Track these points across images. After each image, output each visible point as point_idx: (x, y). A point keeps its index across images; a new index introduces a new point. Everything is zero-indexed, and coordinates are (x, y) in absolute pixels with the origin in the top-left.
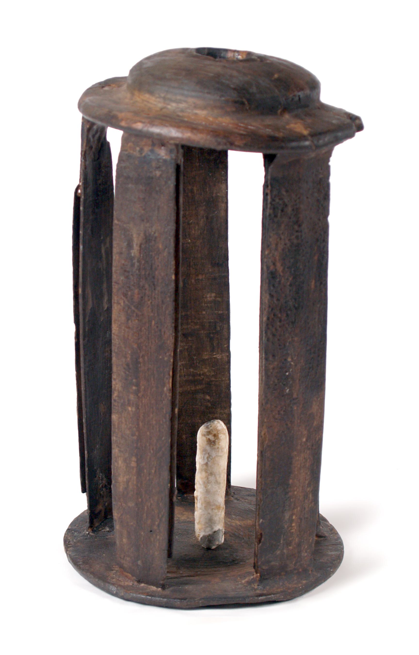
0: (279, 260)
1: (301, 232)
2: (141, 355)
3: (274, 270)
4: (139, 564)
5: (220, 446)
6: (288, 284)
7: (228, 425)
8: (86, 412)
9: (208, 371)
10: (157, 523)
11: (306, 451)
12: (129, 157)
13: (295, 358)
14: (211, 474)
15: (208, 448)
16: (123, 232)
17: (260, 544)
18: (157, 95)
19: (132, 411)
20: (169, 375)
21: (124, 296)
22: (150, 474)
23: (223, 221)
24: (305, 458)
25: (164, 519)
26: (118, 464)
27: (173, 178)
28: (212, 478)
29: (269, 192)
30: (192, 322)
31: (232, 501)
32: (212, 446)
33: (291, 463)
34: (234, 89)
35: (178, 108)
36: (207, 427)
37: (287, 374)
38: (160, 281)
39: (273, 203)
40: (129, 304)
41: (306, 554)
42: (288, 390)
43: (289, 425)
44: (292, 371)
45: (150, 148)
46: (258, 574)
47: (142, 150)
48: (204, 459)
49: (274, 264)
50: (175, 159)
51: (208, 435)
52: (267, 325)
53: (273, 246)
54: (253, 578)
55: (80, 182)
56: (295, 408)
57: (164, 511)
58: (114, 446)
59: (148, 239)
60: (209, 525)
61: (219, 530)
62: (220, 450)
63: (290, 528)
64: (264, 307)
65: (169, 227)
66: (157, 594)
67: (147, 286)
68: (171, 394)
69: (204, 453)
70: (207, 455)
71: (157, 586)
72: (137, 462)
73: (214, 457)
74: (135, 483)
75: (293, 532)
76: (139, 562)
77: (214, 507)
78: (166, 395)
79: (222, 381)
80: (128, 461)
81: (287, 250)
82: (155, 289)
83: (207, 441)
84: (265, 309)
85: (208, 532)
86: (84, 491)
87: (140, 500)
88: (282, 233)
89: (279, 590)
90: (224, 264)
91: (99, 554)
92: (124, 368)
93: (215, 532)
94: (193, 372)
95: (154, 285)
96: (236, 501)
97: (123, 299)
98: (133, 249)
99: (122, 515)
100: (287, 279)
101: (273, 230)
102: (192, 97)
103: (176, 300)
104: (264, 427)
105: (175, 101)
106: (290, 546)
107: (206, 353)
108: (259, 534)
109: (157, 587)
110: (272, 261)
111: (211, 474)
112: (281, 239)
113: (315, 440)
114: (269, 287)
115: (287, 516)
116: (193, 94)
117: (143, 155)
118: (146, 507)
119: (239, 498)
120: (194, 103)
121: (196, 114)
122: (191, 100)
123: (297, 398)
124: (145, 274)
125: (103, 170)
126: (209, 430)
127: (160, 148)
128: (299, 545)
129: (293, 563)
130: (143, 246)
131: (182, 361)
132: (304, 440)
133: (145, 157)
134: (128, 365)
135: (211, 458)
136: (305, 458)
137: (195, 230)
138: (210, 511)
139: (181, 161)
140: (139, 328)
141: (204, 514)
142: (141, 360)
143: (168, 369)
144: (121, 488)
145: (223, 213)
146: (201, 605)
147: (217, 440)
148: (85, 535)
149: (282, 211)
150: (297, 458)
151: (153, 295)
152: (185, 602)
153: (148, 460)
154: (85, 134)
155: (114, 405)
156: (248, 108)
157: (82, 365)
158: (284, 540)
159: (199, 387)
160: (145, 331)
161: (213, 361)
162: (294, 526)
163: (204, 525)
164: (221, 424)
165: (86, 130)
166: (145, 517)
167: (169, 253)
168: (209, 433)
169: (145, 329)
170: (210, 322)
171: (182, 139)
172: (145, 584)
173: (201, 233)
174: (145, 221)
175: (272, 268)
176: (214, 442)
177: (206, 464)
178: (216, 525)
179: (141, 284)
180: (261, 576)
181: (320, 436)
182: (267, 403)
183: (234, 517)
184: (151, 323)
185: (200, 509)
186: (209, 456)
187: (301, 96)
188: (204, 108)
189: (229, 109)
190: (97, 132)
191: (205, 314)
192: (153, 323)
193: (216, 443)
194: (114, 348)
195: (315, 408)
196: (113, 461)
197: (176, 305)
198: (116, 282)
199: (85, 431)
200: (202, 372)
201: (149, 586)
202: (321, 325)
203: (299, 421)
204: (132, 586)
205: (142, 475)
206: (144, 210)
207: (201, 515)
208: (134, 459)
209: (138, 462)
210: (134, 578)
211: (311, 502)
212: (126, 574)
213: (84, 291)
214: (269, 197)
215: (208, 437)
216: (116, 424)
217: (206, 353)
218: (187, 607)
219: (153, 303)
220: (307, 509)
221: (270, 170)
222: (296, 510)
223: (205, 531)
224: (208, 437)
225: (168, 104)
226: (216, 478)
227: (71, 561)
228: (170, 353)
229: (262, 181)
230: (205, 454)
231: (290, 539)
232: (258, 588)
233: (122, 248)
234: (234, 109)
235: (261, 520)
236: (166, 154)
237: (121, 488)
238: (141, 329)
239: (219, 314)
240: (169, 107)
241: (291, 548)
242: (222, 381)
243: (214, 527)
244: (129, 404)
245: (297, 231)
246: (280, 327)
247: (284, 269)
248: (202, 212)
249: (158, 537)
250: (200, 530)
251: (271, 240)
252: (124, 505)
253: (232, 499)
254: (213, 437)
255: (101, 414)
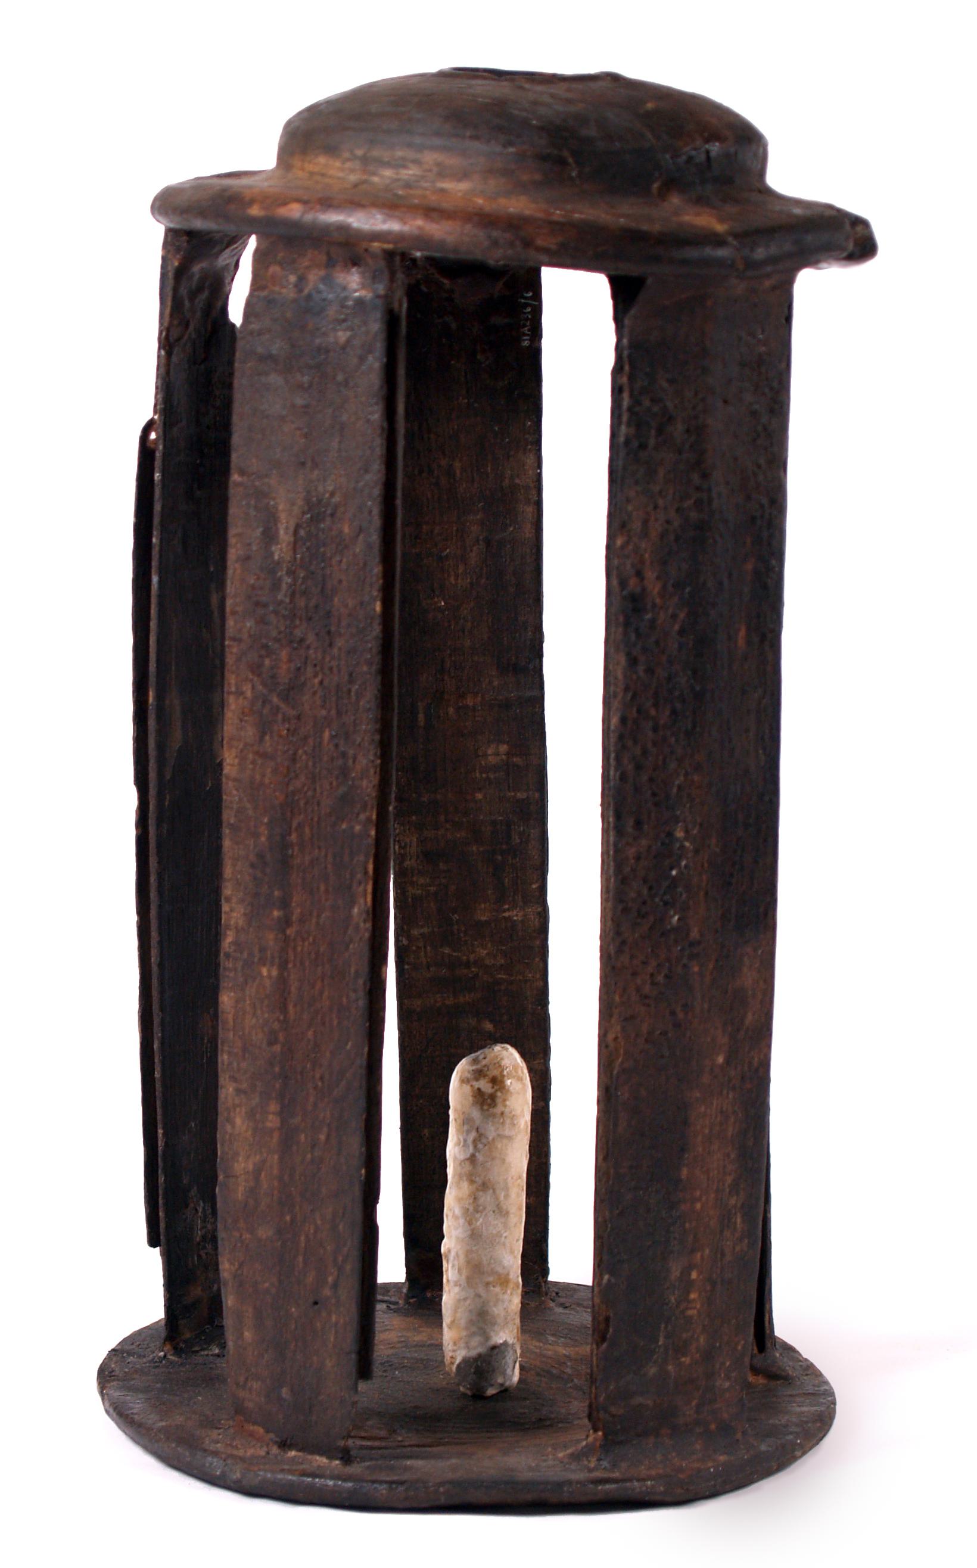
0: (652, 563)
1: (709, 490)
2: (294, 824)
3: (638, 590)
4: (284, 1396)
5: (507, 1110)
6: (677, 627)
7: (542, 1104)
8: (162, 1024)
9: (488, 954)
10: (330, 1279)
11: (725, 1092)
12: (270, 302)
13: (695, 832)
14: (485, 1186)
15: (476, 1114)
16: (253, 502)
17: (605, 1345)
18: (347, 155)
19: (270, 976)
20: (366, 873)
21: (253, 672)
22: (313, 1146)
23: (528, 551)
24: (722, 1112)
25: (348, 1267)
26: (233, 1127)
27: (379, 347)
28: (486, 1198)
29: (624, 380)
30: (447, 821)
31: (551, 1309)
32: (485, 1107)
33: (685, 1122)
34: (542, 129)
35: (398, 180)
36: (475, 1061)
37: (674, 873)
38: (344, 623)
39: (637, 409)
40: (265, 691)
41: (727, 1384)
42: (676, 918)
43: (681, 1015)
44: (686, 866)
45: (322, 273)
46: (600, 1433)
47: (302, 279)
48: (465, 1145)
49: (639, 574)
50: (386, 297)
51: (477, 1080)
52: (621, 737)
53: (636, 526)
54: (587, 1445)
55: (155, 412)
56: (696, 969)
57: (349, 1243)
58: (223, 1079)
59: (316, 512)
60: (481, 1328)
61: (505, 1343)
62: (508, 1121)
63: (683, 1305)
64: (612, 688)
65: (368, 477)
66: (328, 1472)
67: (311, 638)
68: (369, 925)
69: (466, 1127)
70: (473, 1134)
71: (329, 1453)
72: (281, 1113)
73: (491, 1138)
74: (275, 1172)
75: (691, 1317)
76: (285, 1392)
77: (491, 1279)
78: (357, 928)
79: (526, 981)
80: (258, 1116)
81: (672, 537)
82: (331, 645)
83: (474, 1096)
84: (615, 697)
85: (477, 1348)
86: (153, 1242)
87: (288, 1218)
88: (660, 492)
89: (653, 1473)
90: (531, 666)
91: (186, 1396)
92: (252, 866)
93: (494, 1348)
94: (450, 955)
95: (329, 632)
96: (560, 1310)
97: (251, 680)
98: (277, 544)
99: (241, 1265)
100: (674, 616)
101: (637, 483)
102: (433, 148)
103: (385, 672)
104: (613, 1021)
105: (388, 165)
106: (684, 1355)
107: (483, 906)
108: (601, 1318)
109: (331, 1458)
110: (633, 565)
111: (485, 1186)
112: (656, 507)
113: (750, 1063)
114: (625, 633)
115: (675, 1270)
116: (437, 141)
117: (306, 291)
118: (303, 1238)
119: (567, 1305)
120: (438, 164)
121: (443, 191)
122: (430, 158)
123: (699, 943)
124: (307, 607)
125: (217, 393)
126: (479, 1067)
127: (348, 272)
128: (708, 1356)
129: (694, 1403)
130: (302, 533)
131: (422, 927)
132: (720, 1060)
133: (309, 297)
134: (261, 856)
135: (484, 1141)
136: (722, 1112)
137: (457, 576)
138: (481, 1290)
139: (401, 305)
140: (291, 752)
141: (465, 1299)
142: (294, 837)
143: (362, 858)
144: (241, 1189)
145: (528, 531)
146: (443, 1500)
147: (499, 1094)
148: (156, 1359)
149: (660, 431)
150: (703, 1109)
151: (327, 659)
152: (401, 1488)
153: (310, 1108)
154: (171, 282)
155: (224, 968)
156: (574, 174)
157: (153, 895)
158: (667, 1337)
159: (465, 998)
160: (304, 757)
161: (503, 927)
162: (694, 1300)
163: (467, 1328)
164: (512, 1054)
165: (171, 275)
166: (301, 1265)
167: (369, 546)
168: (479, 1074)
169: (306, 753)
170: (494, 823)
171: (400, 237)
172: (300, 1450)
173: (471, 584)
174: (309, 464)
175: (633, 582)
176: (493, 1097)
177: (472, 1159)
178: (496, 1328)
179: (298, 633)
180: (605, 1435)
181: (762, 1057)
182: (620, 951)
183: (551, 1338)
184: (321, 737)
185: (456, 1284)
186: (480, 1136)
187: (713, 154)
188: (464, 175)
189: (525, 178)
190: (199, 289)
191: (480, 801)
192: (326, 735)
193: (499, 1101)
194: (228, 816)
195: (748, 978)
196: (220, 1119)
197: (383, 683)
198: (234, 639)
199: (157, 1075)
200: (472, 957)
201: (310, 1457)
202: (764, 749)
203: (706, 1006)
204: (264, 1457)
205: (295, 1148)
206: (306, 436)
207: (459, 1301)
208: (274, 1107)
209: (285, 1113)
210: (272, 1435)
211: (741, 1240)
212: (251, 1428)
213: (159, 697)
214: (626, 395)
215: (476, 1085)
216: (230, 1017)
217: (483, 906)
218: (407, 1504)
219: (326, 683)
220: (728, 1257)
221: (627, 321)
222: (699, 1255)
223: (467, 1347)
224: (476, 1085)
225: (374, 174)
226: (497, 1198)
227: (111, 1410)
228: (368, 814)
229: (608, 359)
230: (468, 1132)
231: (684, 1335)
232: (594, 1468)
233: (249, 544)
234: (538, 177)
235: (606, 1277)
236: (363, 286)
237: (241, 1189)
238: (295, 754)
239: (518, 801)
240: (376, 179)
241: (686, 1360)
242: (526, 981)
243: (492, 1334)
244: (263, 962)
245: (698, 489)
246: (654, 744)
247: (664, 587)
248: (475, 528)
249: (334, 1318)
250: (455, 1344)
251: (630, 508)
252: (248, 1236)
253: (552, 1304)
254: (490, 1085)
255: (203, 1039)
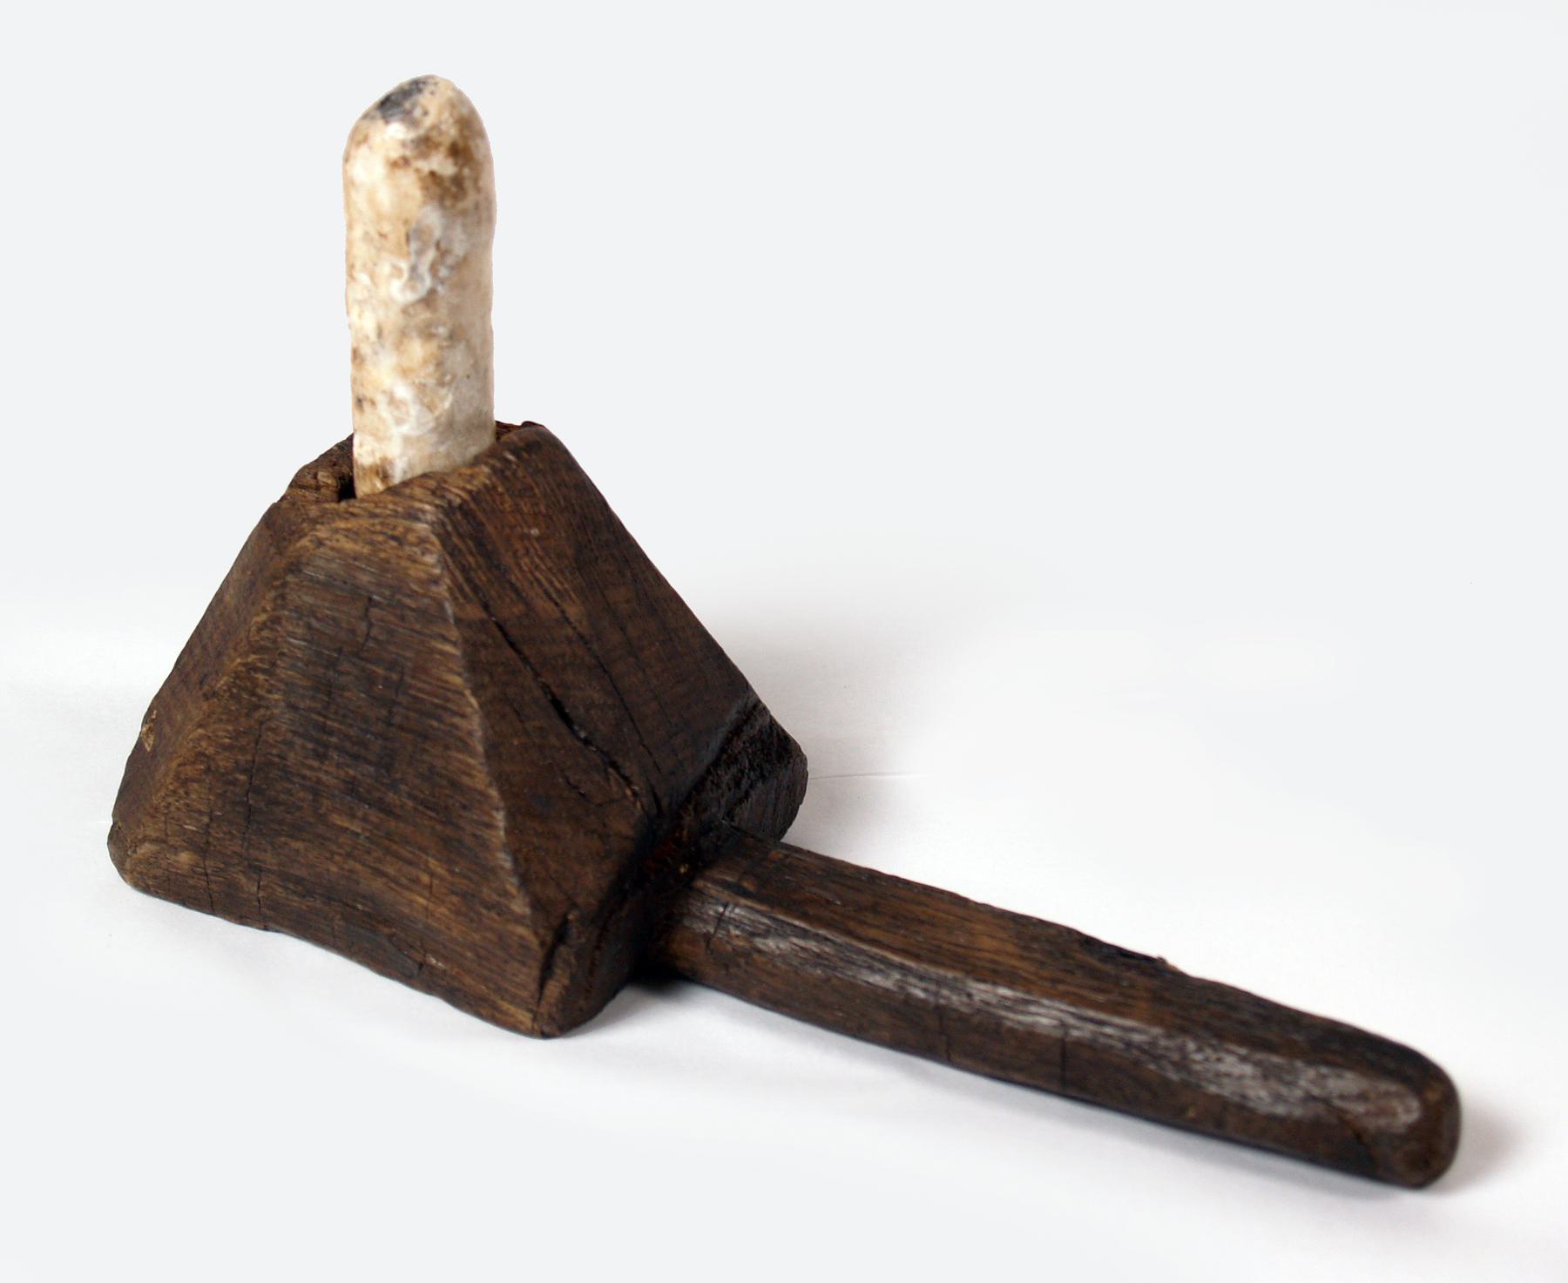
32: (448, 203)
51: (424, 155)
69: (414, 246)
70: (431, 254)
83: (425, 188)
124: (317, 501)
126: (421, 132)
215: (425, 166)
224: (425, 166)
